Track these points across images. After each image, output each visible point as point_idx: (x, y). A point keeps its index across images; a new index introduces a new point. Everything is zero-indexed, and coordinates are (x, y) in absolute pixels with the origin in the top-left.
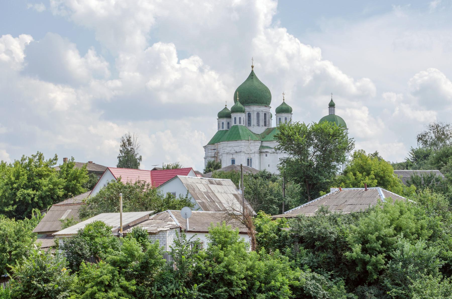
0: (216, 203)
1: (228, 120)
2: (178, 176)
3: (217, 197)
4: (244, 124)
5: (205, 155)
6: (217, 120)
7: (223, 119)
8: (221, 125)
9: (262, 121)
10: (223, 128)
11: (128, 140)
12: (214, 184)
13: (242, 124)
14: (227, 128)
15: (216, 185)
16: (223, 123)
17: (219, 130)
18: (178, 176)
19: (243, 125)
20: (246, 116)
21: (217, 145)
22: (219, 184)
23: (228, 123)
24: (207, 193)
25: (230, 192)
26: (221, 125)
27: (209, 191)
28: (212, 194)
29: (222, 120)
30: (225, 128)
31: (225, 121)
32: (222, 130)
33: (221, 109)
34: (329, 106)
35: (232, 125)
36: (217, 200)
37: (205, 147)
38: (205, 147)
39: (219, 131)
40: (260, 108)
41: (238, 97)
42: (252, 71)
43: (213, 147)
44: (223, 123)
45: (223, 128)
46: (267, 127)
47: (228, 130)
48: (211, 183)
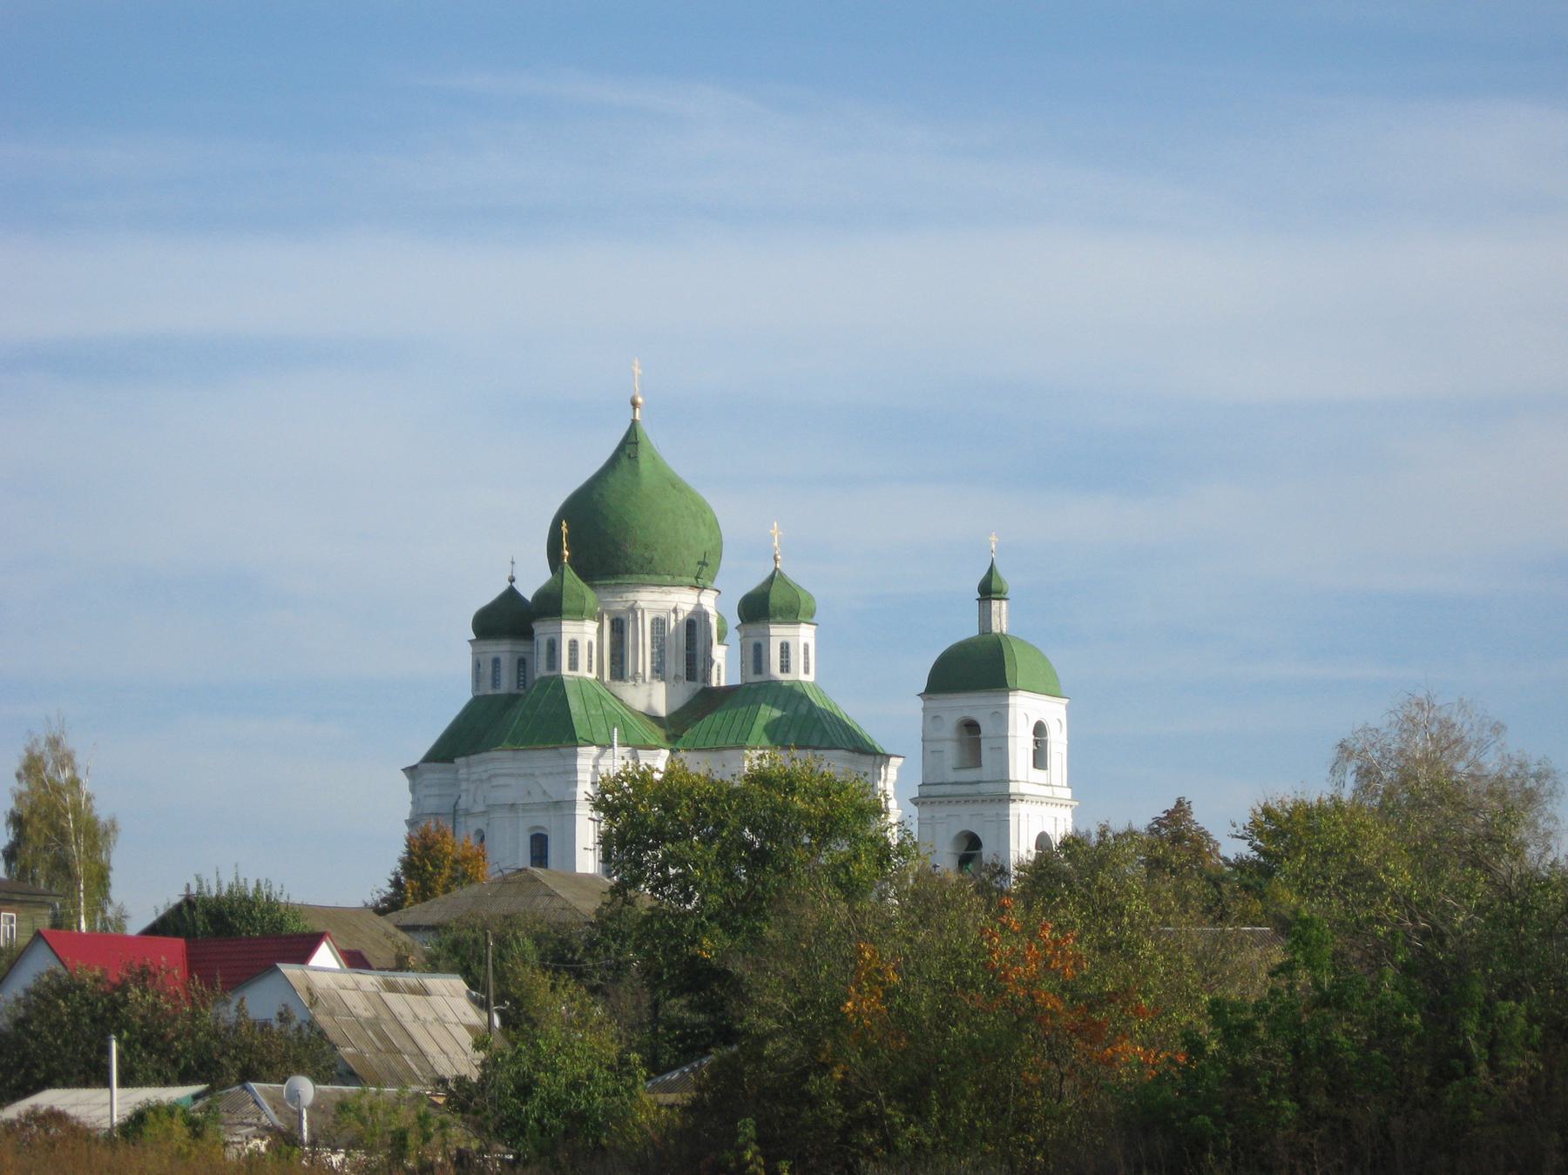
0: (406, 1057)
1: (521, 647)
2: (279, 965)
3: (410, 1036)
4: (590, 671)
5: (409, 808)
6: (470, 649)
7: (495, 642)
8: (488, 669)
9: (677, 655)
10: (496, 682)
11: (54, 743)
12: (400, 992)
13: (583, 671)
14: (515, 684)
15: (407, 996)
16: (496, 661)
17: (480, 694)
18: (279, 965)
19: (588, 675)
20: (600, 631)
21: (468, 766)
22: (424, 991)
23: (522, 664)
24: (374, 1023)
25: (455, 1020)
26: (489, 671)
27: (386, 1016)
28: (393, 1026)
29: (494, 648)
30: (507, 685)
31: (503, 649)
32: (490, 692)
33: (490, 593)
34: (979, 596)
35: (537, 676)
36: (409, 1047)
37: (411, 771)
38: (411, 771)
39: (476, 701)
40: (670, 598)
41: (565, 545)
42: (634, 422)
43: (438, 773)
44: (496, 661)
45: (496, 682)
46: (699, 685)
47: (522, 692)
48: (392, 988)
